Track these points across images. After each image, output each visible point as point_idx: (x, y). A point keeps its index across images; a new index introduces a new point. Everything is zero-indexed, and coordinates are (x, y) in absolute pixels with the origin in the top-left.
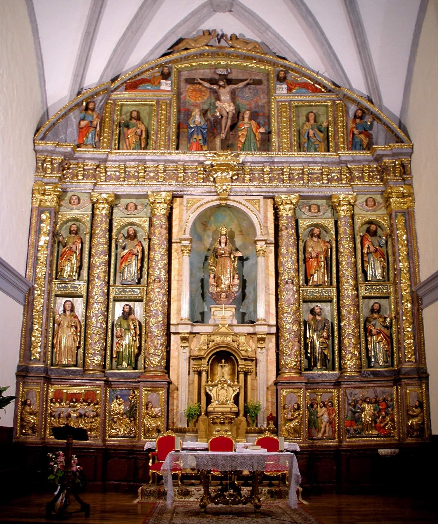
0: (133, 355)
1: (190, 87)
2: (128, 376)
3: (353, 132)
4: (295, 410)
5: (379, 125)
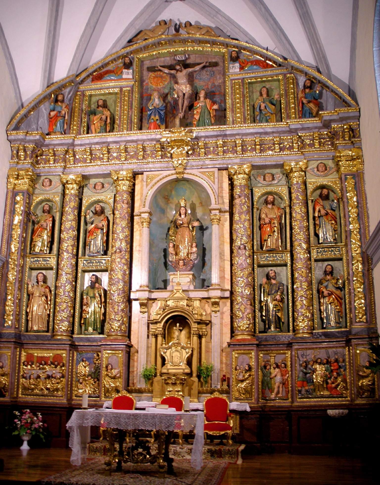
0: (98, 321)
1: (152, 74)
2: (94, 340)
3: (302, 101)
4: (247, 371)
5: (328, 93)
